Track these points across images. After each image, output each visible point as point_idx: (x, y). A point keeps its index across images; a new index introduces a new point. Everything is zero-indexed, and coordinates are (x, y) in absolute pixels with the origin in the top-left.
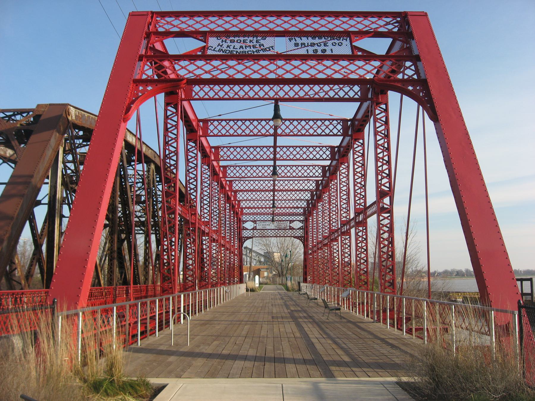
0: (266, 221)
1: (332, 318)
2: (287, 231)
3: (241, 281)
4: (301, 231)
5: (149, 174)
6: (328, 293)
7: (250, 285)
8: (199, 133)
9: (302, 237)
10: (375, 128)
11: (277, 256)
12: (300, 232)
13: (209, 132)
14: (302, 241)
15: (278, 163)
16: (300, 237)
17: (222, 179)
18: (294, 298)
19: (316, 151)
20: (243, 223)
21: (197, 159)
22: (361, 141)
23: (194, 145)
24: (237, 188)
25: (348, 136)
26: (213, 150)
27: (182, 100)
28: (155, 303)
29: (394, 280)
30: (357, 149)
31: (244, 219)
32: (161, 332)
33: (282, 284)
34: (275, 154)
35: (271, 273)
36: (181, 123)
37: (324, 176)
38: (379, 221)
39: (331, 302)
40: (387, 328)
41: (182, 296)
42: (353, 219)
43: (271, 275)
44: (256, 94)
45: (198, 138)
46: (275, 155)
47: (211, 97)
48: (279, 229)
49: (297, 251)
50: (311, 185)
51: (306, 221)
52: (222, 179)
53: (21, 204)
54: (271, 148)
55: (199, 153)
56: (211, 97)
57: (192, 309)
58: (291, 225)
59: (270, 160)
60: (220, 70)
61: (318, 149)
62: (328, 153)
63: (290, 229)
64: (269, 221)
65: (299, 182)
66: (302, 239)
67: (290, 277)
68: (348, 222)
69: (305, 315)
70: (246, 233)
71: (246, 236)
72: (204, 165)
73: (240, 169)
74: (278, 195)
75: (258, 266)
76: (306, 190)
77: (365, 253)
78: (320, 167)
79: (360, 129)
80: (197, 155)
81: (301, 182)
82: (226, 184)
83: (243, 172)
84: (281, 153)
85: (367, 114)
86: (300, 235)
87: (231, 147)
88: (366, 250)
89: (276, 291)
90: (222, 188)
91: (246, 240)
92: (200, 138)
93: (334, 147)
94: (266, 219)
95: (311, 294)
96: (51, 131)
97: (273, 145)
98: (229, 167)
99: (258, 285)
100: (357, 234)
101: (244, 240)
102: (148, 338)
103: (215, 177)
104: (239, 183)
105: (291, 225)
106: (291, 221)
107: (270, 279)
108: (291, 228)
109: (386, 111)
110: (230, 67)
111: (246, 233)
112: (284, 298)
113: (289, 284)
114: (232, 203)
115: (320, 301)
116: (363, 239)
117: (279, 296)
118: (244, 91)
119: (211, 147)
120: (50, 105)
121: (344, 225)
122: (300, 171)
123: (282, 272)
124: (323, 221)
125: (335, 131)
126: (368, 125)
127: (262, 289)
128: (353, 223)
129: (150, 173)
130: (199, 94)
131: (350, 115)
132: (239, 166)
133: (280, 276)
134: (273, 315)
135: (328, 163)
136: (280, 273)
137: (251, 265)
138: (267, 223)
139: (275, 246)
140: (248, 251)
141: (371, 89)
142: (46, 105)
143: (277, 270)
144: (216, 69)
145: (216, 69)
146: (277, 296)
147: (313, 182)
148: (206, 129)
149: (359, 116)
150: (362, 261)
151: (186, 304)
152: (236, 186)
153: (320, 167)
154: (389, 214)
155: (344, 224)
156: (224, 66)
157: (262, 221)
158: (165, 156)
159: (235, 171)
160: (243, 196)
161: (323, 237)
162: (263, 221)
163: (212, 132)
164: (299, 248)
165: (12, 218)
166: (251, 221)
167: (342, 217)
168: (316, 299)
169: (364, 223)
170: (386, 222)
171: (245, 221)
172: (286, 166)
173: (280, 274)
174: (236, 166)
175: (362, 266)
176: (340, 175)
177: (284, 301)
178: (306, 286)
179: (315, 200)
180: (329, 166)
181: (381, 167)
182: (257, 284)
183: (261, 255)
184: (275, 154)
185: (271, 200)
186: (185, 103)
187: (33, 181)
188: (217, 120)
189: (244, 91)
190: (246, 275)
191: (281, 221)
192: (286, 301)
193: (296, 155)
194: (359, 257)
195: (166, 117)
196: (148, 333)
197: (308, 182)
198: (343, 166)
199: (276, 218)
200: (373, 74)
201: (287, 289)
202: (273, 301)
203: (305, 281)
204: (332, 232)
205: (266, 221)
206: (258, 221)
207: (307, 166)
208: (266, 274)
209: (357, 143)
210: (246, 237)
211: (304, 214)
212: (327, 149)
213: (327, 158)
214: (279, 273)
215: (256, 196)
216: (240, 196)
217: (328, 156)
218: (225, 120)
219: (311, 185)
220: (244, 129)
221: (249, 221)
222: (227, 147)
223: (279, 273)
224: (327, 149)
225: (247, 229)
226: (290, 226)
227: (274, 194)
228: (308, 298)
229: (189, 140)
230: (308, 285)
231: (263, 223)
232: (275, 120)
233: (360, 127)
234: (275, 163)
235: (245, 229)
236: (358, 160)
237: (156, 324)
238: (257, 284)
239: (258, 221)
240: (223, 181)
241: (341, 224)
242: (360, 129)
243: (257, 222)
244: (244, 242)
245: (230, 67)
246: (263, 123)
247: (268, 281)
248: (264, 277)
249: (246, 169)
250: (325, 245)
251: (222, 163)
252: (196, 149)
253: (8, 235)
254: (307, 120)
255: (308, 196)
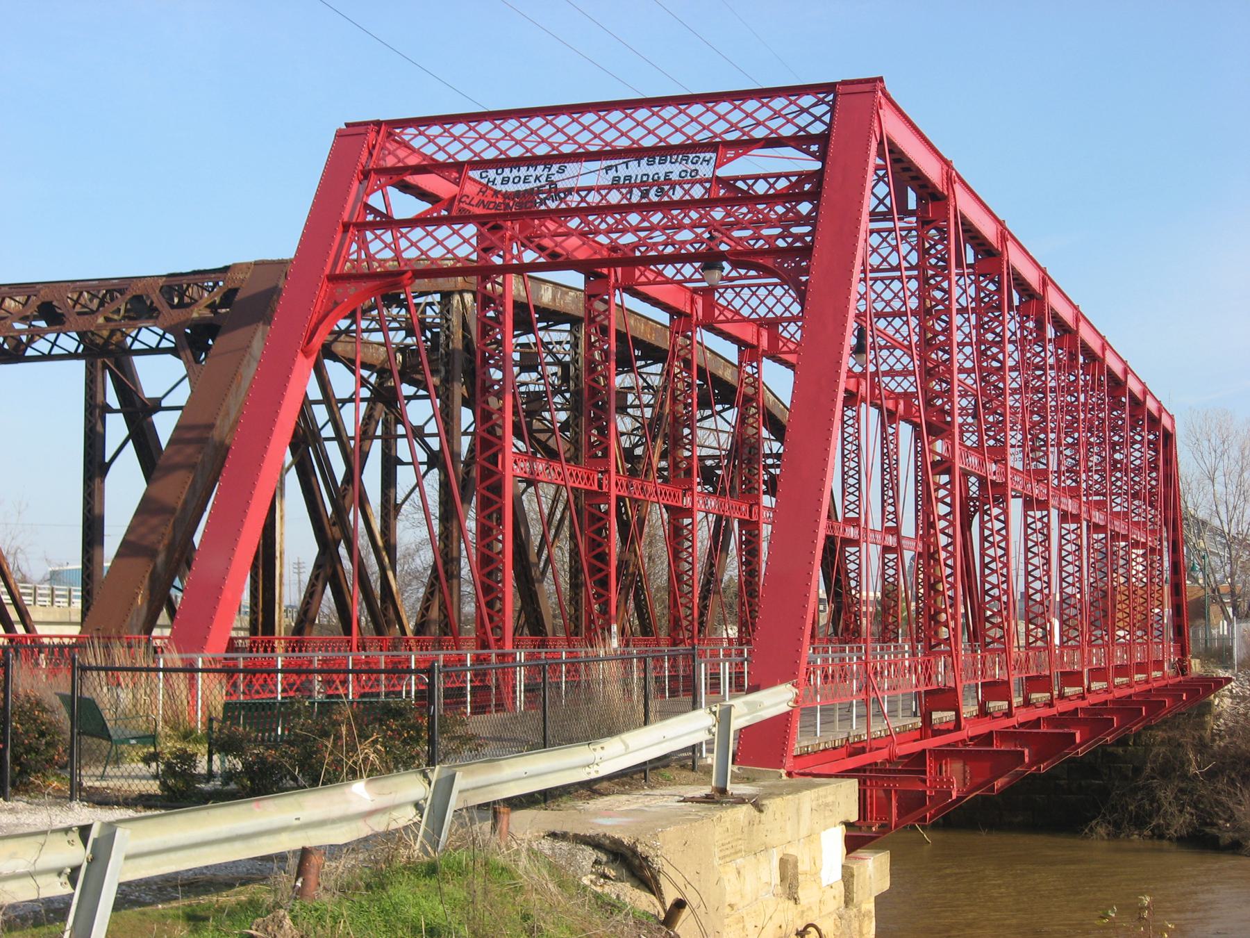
5: (576, 353)
53: (189, 483)
60: (784, 116)
73: (754, 293)
83: (779, 301)
96: (255, 326)
101: (974, 506)
110: (803, 110)
120: (257, 264)
129: (579, 351)
142: (248, 266)
144: (746, 129)
145: (746, 129)
156: (793, 108)
165: (172, 511)
187: (216, 435)
200: (790, 181)
245: (803, 110)
253: (166, 542)
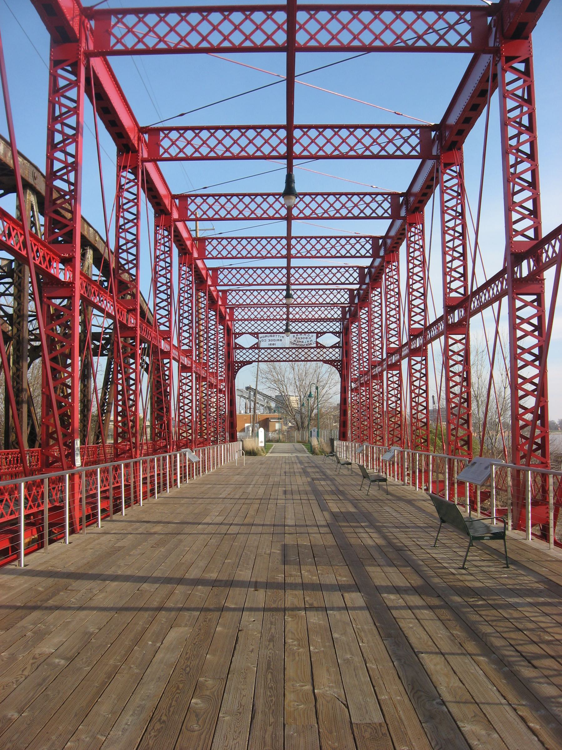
0: (276, 333)
1: (374, 491)
2: (312, 350)
3: (233, 438)
4: (337, 350)
6: (402, 466)
7: (250, 444)
8: (83, 45)
9: (339, 361)
10: (443, 202)
11: (294, 401)
12: (334, 353)
13: (161, 153)
14: (337, 368)
15: (294, 262)
16: (335, 361)
17: (212, 288)
18: (329, 472)
19: (350, 244)
20: (236, 338)
21: (170, 256)
22: (379, 290)
23: (132, 177)
24: (234, 301)
25: (399, 218)
26: (210, 272)
27: (144, 160)
28: (96, 474)
29: (469, 436)
30: (448, 184)
31: (237, 331)
32: (146, 501)
33: (302, 442)
34: (289, 276)
35: (286, 424)
36: (143, 196)
37: (361, 282)
38: (513, 310)
39: (373, 469)
40: (395, 480)
41: (178, 455)
42: (406, 344)
43: (285, 428)
44: (247, 38)
45: (140, 164)
46: (290, 146)
47: (189, 155)
48: (299, 348)
49: (324, 391)
50: (342, 296)
51: (345, 333)
52: (212, 288)
54: (284, 269)
55: (141, 191)
56: (189, 155)
57: (189, 471)
58: (318, 340)
59: (283, 257)
61: (353, 241)
62: (356, 275)
63: (317, 347)
64: (280, 333)
65: (324, 293)
66: (337, 365)
67: (316, 430)
68: (398, 351)
69: (318, 470)
70: (241, 354)
71: (241, 359)
72: (184, 266)
74: (294, 312)
75: (267, 414)
76: (335, 304)
77: (424, 395)
78: (346, 290)
79: (470, 118)
80: (137, 195)
81: (328, 292)
82: (218, 295)
84: (299, 247)
85: (430, 184)
86: (334, 358)
87: (223, 239)
88: (426, 391)
89: (294, 455)
90: (185, 254)
91: (241, 367)
92: (88, 62)
93: (378, 238)
94: (275, 330)
95: (356, 461)
97: (286, 266)
98: (221, 270)
99: (263, 445)
100: (410, 367)
101: (238, 366)
102: (46, 548)
103: (163, 217)
104: (237, 294)
105: (318, 340)
106: (319, 333)
107: (283, 434)
108: (320, 346)
109: (460, 176)
111: (241, 354)
112: (309, 470)
113: (315, 442)
114: (227, 324)
115: (355, 467)
116: (422, 375)
117: (299, 465)
118: (220, 32)
119: (174, 197)
121: (392, 354)
122: (326, 275)
123: (303, 423)
124: (360, 350)
125: (363, 252)
126: (430, 202)
127: (270, 451)
128: (405, 351)
130: (166, 139)
131: (382, 233)
132: (236, 268)
133: (298, 429)
134: (289, 540)
135: (367, 262)
136: (300, 424)
137: (254, 412)
138: (277, 337)
139: (291, 384)
140: (252, 393)
141: (494, 29)
143: (294, 419)
146: (295, 466)
147: (346, 292)
148: (154, 145)
149: (417, 188)
150: (421, 408)
151: (183, 465)
152: (232, 299)
153: (346, 290)
154: (464, 336)
155: (391, 353)
157: (268, 333)
158: (118, 247)
159: (230, 276)
160: (243, 313)
161: (361, 373)
162: (269, 333)
163: (210, 253)
164: (328, 385)
166: (249, 333)
167: (412, 322)
168: (350, 464)
169: (422, 351)
170: (457, 347)
171: (238, 334)
172: (308, 237)
173: (300, 427)
174: (232, 268)
175: (421, 416)
176: (386, 280)
177: (309, 479)
178: (347, 446)
179: (367, 284)
180: (369, 268)
181: (450, 263)
182: (262, 442)
183: (270, 398)
184: (289, 276)
185: (283, 320)
186: (149, 166)
188: (201, 196)
189: (220, 32)
190: (248, 427)
191: (301, 333)
192: (313, 479)
193: (320, 250)
194: (415, 402)
195: (120, 188)
196: (46, 539)
197: (339, 293)
198: (353, 325)
199: (293, 327)
201: (312, 451)
202: (288, 467)
203: (343, 436)
204: (374, 365)
205: (276, 333)
206: (261, 333)
207: (336, 267)
208: (277, 426)
209: (448, 171)
210: (241, 362)
211: (342, 319)
212: (367, 242)
213: (412, 154)
214: (297, 425)
215: (262, 313)
216: (232, 299)
217: (355, 279)
218: (213, 196)
219: (342, 296)
220: (241, 209)
221: (245, 333)
222: (217, 239)
223: (297, 425)
224: (367, 242)
225: (243, 348)
226: (317, 343)
227: (288, 311)
228: (339, 462)
229: (121, 168)
230: (349, 444)
231: (269, 338)
232: (286, 197)
233: (418, 205)
234: (289, 263)
235: (239, 348)
236: (449, 204)
237: (125, 500)
238: (262, 442)
239: (261, 333)
240: (214, 291)
241: (387, 353)
242: (470, 118)
243: (260, 335)
244: (238, 369)
246: (274, 242)
247: (281, 436)
248: (276, 431)
249: (252, 293)
250: (374, 377)
251: (210, 264)
252: (137, 184)
254: (338, 195)
255: (337, 313)
